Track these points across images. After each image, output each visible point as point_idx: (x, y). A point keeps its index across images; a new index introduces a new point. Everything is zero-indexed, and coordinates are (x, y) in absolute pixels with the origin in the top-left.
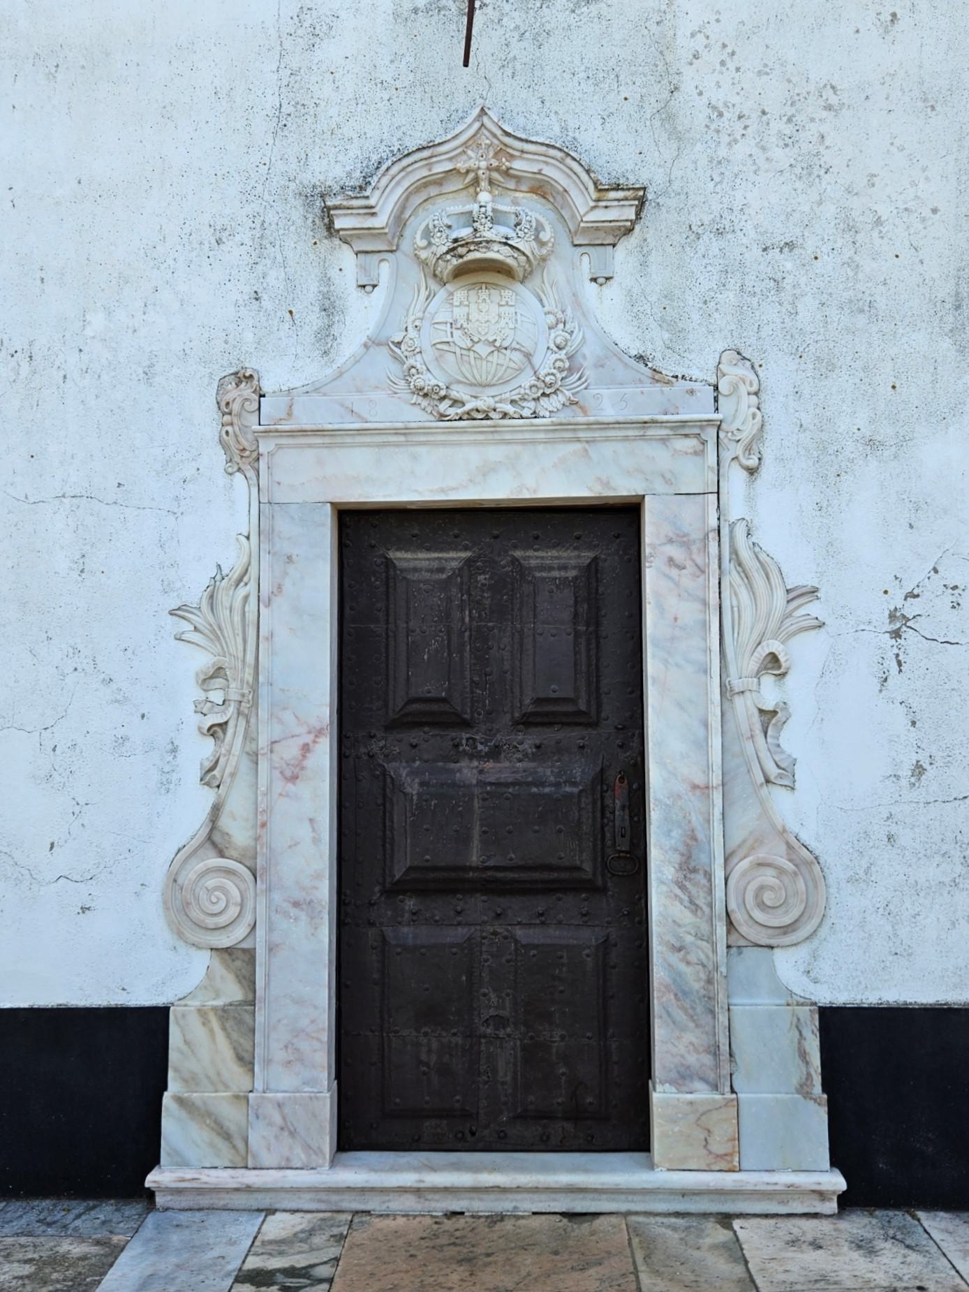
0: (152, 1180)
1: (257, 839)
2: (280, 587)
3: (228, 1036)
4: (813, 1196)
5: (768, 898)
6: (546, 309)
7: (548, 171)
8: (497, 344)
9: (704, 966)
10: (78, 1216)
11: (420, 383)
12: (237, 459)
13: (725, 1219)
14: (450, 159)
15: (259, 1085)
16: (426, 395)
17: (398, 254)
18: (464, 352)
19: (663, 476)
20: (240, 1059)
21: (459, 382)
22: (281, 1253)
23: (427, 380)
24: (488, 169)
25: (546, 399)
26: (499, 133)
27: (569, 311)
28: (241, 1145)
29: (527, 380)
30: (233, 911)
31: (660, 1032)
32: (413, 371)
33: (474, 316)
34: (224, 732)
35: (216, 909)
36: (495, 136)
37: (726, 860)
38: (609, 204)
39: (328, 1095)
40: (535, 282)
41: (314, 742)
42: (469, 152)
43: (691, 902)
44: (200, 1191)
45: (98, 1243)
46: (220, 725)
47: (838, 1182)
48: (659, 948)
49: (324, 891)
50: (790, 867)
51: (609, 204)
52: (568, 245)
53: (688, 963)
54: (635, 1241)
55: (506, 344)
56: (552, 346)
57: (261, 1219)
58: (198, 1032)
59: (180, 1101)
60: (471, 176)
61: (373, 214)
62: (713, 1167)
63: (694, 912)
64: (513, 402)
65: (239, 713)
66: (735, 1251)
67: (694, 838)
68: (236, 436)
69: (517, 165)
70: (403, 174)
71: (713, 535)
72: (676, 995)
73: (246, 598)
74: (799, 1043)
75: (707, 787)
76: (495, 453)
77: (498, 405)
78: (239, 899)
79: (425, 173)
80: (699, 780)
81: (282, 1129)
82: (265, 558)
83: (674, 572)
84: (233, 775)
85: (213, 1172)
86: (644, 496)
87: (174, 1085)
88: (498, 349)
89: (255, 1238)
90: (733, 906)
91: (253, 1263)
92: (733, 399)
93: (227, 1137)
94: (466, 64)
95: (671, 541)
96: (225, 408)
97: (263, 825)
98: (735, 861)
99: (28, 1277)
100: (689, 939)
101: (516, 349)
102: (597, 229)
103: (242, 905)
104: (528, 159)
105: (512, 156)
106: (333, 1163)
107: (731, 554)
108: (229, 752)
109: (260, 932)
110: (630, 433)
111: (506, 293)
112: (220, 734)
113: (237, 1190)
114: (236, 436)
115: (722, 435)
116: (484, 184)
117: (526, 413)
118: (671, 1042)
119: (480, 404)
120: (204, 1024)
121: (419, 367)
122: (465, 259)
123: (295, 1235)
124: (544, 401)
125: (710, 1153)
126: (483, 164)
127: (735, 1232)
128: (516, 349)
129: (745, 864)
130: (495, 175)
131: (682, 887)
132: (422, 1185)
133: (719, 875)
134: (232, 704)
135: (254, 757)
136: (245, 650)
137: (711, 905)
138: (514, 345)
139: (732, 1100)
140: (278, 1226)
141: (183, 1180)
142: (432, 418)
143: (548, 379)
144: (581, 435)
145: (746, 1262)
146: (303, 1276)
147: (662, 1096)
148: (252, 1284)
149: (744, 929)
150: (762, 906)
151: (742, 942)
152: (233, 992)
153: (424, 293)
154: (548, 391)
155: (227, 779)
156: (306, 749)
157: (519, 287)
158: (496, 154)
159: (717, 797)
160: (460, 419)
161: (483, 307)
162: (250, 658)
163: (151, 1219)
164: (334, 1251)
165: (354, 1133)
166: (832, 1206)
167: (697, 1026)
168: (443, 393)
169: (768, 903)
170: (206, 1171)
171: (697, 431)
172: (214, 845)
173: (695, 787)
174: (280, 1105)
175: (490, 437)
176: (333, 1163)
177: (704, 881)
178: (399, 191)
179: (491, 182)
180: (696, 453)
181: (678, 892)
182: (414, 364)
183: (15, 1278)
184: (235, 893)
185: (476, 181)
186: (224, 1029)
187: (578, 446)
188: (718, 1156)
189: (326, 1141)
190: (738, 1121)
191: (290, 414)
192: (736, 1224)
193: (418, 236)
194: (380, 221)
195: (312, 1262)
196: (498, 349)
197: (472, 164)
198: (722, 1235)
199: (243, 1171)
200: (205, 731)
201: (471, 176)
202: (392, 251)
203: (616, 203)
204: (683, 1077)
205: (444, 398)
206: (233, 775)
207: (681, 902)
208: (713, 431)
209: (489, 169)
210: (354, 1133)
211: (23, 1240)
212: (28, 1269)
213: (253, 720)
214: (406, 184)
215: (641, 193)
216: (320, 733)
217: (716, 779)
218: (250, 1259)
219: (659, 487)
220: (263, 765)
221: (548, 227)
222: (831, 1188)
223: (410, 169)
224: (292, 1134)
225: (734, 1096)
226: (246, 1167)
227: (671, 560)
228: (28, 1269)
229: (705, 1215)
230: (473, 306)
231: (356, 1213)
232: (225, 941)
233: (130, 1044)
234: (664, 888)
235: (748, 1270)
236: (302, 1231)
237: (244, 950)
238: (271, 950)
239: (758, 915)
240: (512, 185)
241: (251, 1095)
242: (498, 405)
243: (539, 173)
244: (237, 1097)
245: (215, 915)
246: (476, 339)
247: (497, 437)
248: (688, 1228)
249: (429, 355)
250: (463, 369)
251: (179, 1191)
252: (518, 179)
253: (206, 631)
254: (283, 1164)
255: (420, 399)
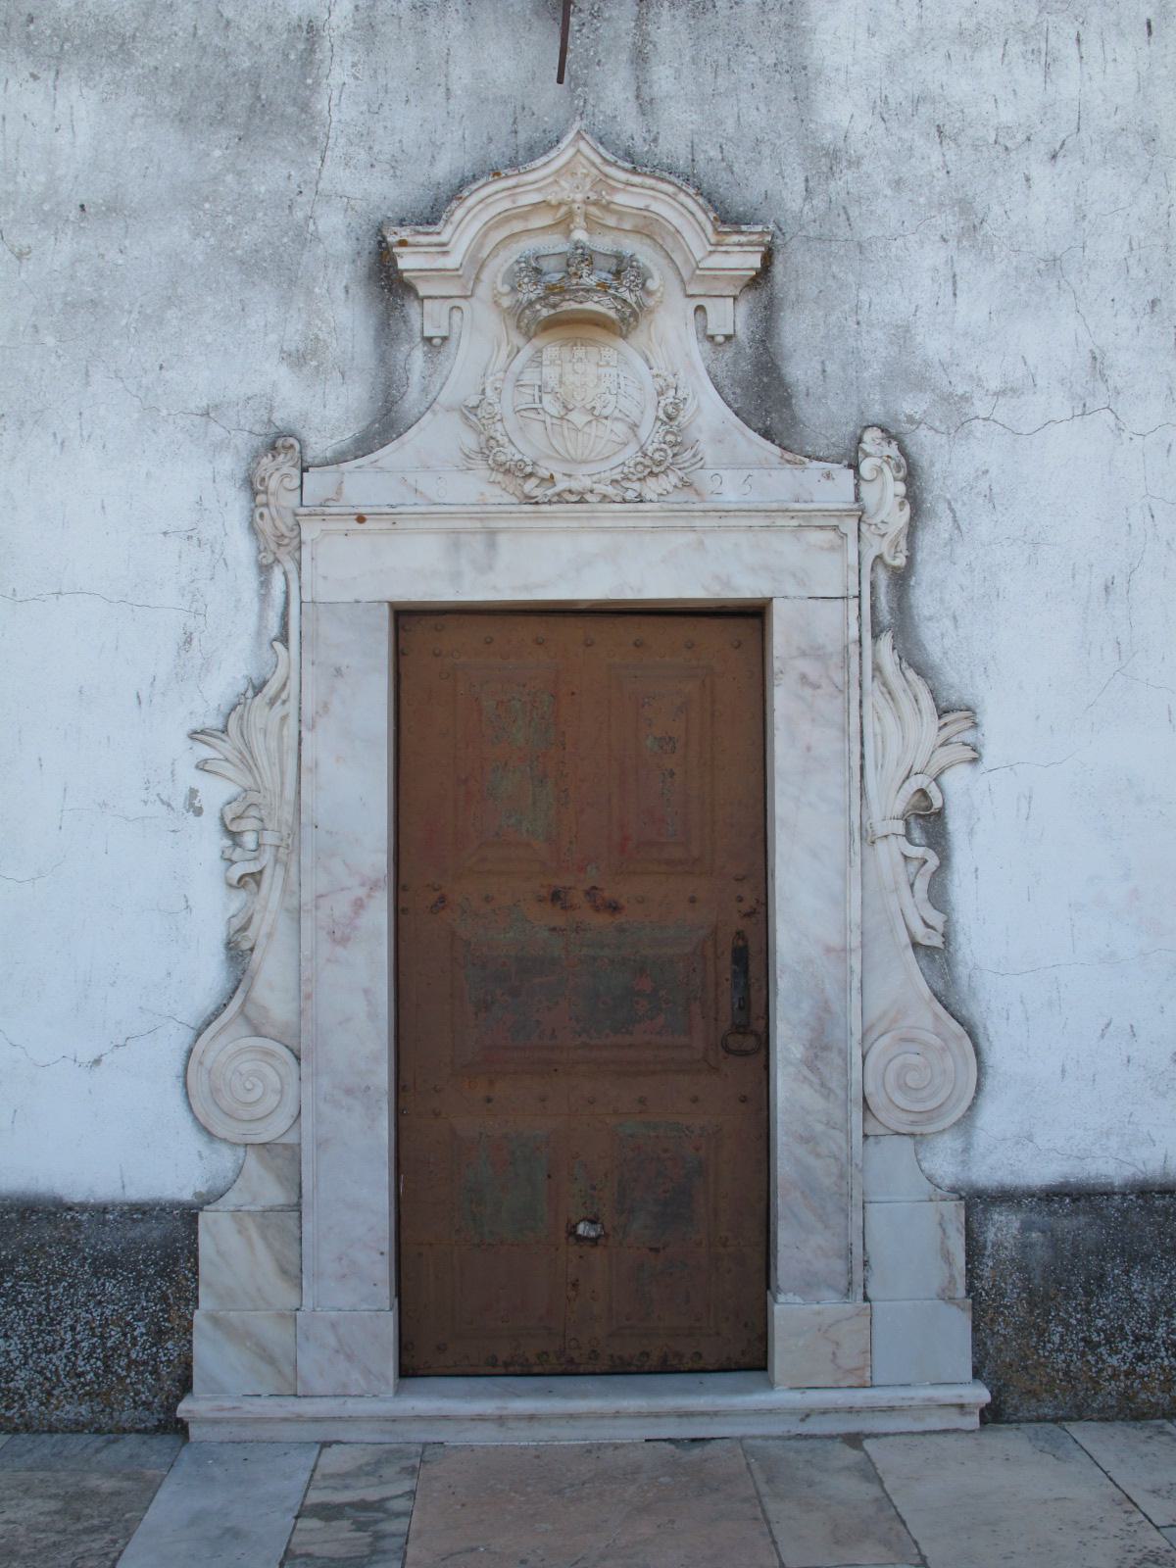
0: (184, 1409)
1: (300, 1013)
2: (326, 706)
3: (269, 1246)
4: (953, 1410)
5: (912, 1080)
6: (655, 371)
7: (656, 207)
8: (596, 413)
9: (837, 1159)
10: (98, 1451)
11: (502, 458)
12: (273, 546)
13: (854, 1440)
14: (539, 190)
15: (308, 1303)
16: (508, 471)
17: (473, 300)
18: (555, 421)
19: (794, 576)
20: (284, 1272)
21: (549, 457)
22: (346, 1487)
23: (508, 454)
24: (585, 202)
25: (654, 479)
26: (598, 161)
27: (681, 374)
28: (288, 1370)
29: (630, 454)
30: (272, 1100)
31: (785, 1236)
32: (492, 443)
33: (569, 378)
34: (258, 884)
35: (252, 1097)
36: (593, 164)
37: (864, 1035)
38: (730, 249)
39: (391, 1313)
40: (639, 337)
41: (369, 896)
42: (563, 183)
43: (823, 1085)
44: (243, 1422)
45: (128, 1477)
46: (252, 874)
47: (982, 1395)
48: (784, 1138)
49: (382, 1076)
50: (937, 1042)
51: (730, 249)
52: (679, 295)
53: (818, 1155)
54: (755, 1466)
55: (606, 412)
56: (662, 416)
57: (316, 1452)
58: (233, 1241)
59: (215, 1320)
60: (564, 209)
61: (445, 253)
62: (842, 1384)
63: (827, 1097)
64: (614, 482)
65: (276, 861)
66: (870, 1473)
67: (827, 1009)
68: (273, 519)
69: (620, 199)
70: (481, 206)
71: (854, 649)
72: (802, 1192)
73: (284, 719)
74: (942, 1243)
75: (844, 950)
76: (590, 543)
77: (595, 486)
78: (279, 1086)
79: (507, 204)
80: (835, 941)
81: (337, 1352)
82: (308, 669)
83: (808, 692)
84: (270, 935)
85: (256, 1400)
86: (771, 599)
87: (206, 1301)
88: (597, 418)
89: (314, 1470)
90: (870, 1089)
91: (315, 1497)
92: (877, 485)
93: (271, 1360)
94: (560, 80)
95: (803, 654)
96: (253, 486)
97: (309, 997)
98: (874, 1035)
99: (56, 1512)
100: (819, 1128)
101: (617, 419)
102: (715, 277)
103: (282, 1092)
104: (632, 193)
105: (614, 189)
106: (398, 1392)
107: (874, 670)
108: (265, 908)
109: (307, 1122)
110: (754, 522)
111: (607, 352)
112: (252, 885)
113: (285, 1420)
114: (273, 519)
115: (864, 527)
116: (579, 220)
117: (631, 495)
118: (799, 1244)
119: (575, 485)
120: (240, 1232)
121: (499, 438)
122: (559, 310)
123: (360, 1468)
124: (651, 482)
125: (839, 1367)
126: (579, 197)
127: (866, 1453)
128: (617, 419)
129: (885, 1040)
130: (593, 210)
131: (812, 1068)
132: (505, 1413)
133: (857, 1053)
134: (267, 848)
135: (297, 914)
136: (282, 784)
137: (847, 1087)
138: (617, 414)
139: (866, 1309)
140: (334, 1460)
141: (222, 1410)
142: (507, 498)
143: (657, 456)
144: (697, 523)
145: (881, 1482)
146: (377, 1510)
147: (788, 1312)
148: (321, 1519)
149: (882, 1115)
150: (903, 1087)
151: (881, 1131)
152: (274, 1194)
153: (505, 350)
154: (656, 470)
155: (262, 940)
156: (359, 905)
157: (620, 343)
158: (594, 184)
159: (855, 962)
160: (550, 502)
161: (579, 367)
162: (290, 793)
163: (185, 1455)
164: (407, 1485)
165: (414, 1363)
166: (974, 1421)
167: (826, 1227)
168: (529, 470)
169: (911, 1083)
170: (249, 1399)
171: (834, 522)
172: (248, 1020)
173: (828, 950)
174: (334, 1326)
175: (585, 524)
176: (398, 1392)
177: (838, 1061)
178: (477, 225)
179: (587, 217)
180: (832, 549)
181: (806, 1072)
182: (494, 434)
183: (41, 1514)
184: (273, 1078)
185: (570, 214)
186: (264, 1238)
187: (691, 537)
188: (901, 579)
189: (390, 1368)
190: (870, 1320)
191: (339, 492)
192: (868, 1444)
193: (499, 280)
194: (451, 262)
195: (385, 1496)
196: (597, 418)
197: (564, 196)
198: (852, 1455)
199: (293, 1399)
200: (235, 882)
201: (564, 209)
202: (465, 297)
203: (738, 249)
204: (809, 1286)
205: (531, 475)
206: (270, 935)
207: (811, 1084)
208: (853, 523)
209: (587, 201)
210: (414, 1363)
211: (41, 1475)
212: (53, 1505)
213: (293, 870)
214: (485, 217)
215: (769, 238)
216: (374, 887)
217: (855, 940)
218: (310, 1493)
219: (791, 589)
220: (307, 924)
221: (656, 274)
222: (973, 1401)
223: (490, 200)
224: (350, 1358)
225: (868, 1304)
226: (295, 1395)
227: (804, 678)
228: (53, 1505)
229: (831, 1437)
230: (568, 367)
231: (425, 1445)
232: (268, 1133)
233: (149, 1256)
234: (791, 1070)
235: (884, 1491)
236: (368, 1464)
237: (285, 1145)
238: (319, 1146)
239: (900, 1100)
240: (611, 221)
241: (298, 1313)
242: (595, 486)
243: (646, 209)
244: (282, 1316)
245: (250, 1104)
246: (570, 407)
247: (595, 523)
248: (812, 1450)
249: (511, 422)
250: (554, 442)
251: (215, 1422)
252: (621, 215)
253: (236, 761)
254: (339, 1391)
255: (500, 477)
